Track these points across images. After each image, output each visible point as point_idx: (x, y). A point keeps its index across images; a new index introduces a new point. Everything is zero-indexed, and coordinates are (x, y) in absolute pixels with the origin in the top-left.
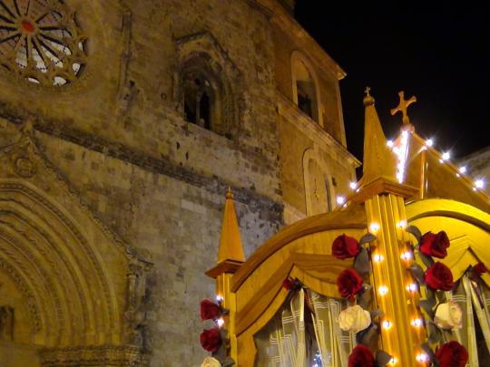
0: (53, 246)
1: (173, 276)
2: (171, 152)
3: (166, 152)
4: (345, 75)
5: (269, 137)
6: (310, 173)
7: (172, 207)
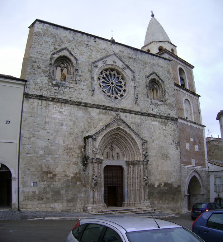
0: (126, 139)
1: (152, 142)
2: (148, 110)
3: (147, 110)
4: (189, 149)
5: (173, 99)
6: (185, 104)
7: (150, 124)
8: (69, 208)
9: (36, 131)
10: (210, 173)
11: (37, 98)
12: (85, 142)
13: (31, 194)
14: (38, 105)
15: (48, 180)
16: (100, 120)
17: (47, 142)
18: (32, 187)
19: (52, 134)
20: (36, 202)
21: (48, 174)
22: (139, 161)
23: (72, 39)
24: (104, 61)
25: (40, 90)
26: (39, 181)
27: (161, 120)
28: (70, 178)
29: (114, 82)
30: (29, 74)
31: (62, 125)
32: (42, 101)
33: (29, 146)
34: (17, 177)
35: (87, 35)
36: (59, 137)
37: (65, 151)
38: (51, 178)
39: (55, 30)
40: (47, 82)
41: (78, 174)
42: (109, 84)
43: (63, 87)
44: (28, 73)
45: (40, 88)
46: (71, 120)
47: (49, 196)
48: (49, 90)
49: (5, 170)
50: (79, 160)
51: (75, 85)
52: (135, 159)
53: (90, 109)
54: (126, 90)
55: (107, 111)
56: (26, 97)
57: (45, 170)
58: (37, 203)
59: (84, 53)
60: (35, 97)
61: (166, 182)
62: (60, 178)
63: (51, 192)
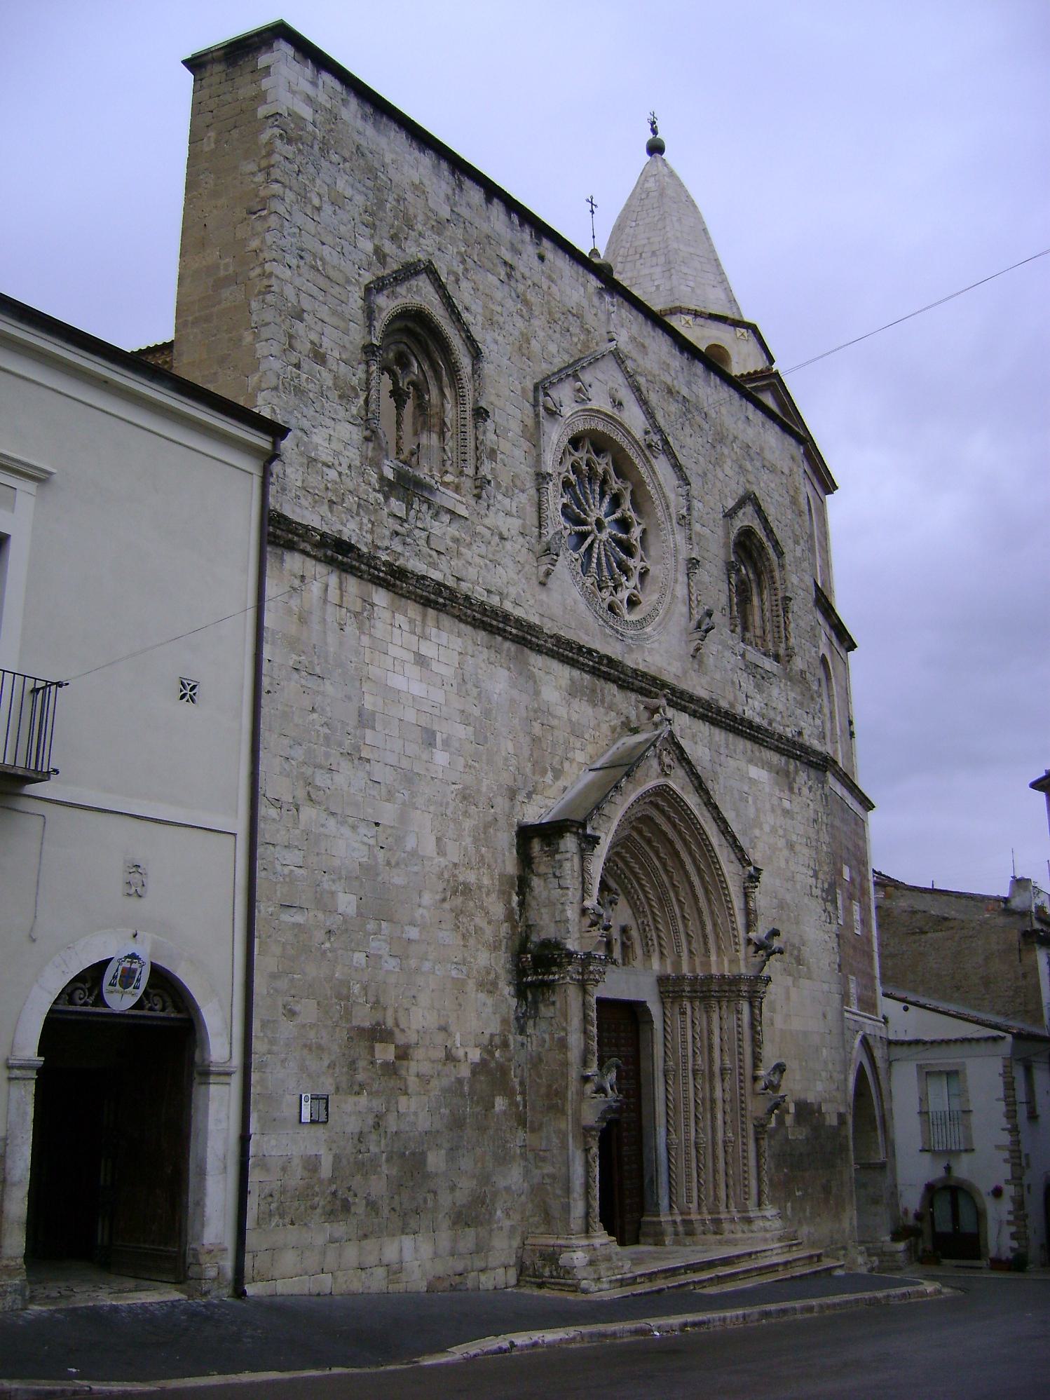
0: (676, 854)
8: (460, 1267)
9: (321, 767)
10: (898, 1052)
11: (320, 554)
12: (525, 859)
13: (296, 1178)
14: (325, 601)
15: (375, 1086)
16: (576, 731)
17: (372, 842)
18: (305, 1131)
19: (390, 797)
20: (319, 1233)
21: (378, 1046)
22: (736, 980)
23: (445, 212)
24: (579, 390)
25: (331, 502)
26: (337, 1089)
27: (775, 758)
28: (465, 1071)
29: (607, 515)
30: (276, 388)
31: (429, 739)
32: (340, 578)
33: (293, 857)
34: (237, 1061)
35: (512, 206)
36: (419, 812)
37: (444, 900)
38: (391, 1070)
39: (370, 130)
40: (353, 455)
41: (497, 1047)
42: (584, 523)
43: (425, 507)
44: (274, 382)
45: (330, 494)
46: (466, 718)
47: (378, 1186)
48: (367, 511)
49: (163, 1010)
50: (496, 962)
51: (472, 502)
52: (707, 964)
53: (537, 662)
54: (647, 571)
55: (600, 683)
56: (270, 543)
57: (363, 1016)
58: (320, 1240)
59: (501, 320)
60: (317, 545)
61: (802, 1097)
62: (426, 1068)
63: (388, 1160)
